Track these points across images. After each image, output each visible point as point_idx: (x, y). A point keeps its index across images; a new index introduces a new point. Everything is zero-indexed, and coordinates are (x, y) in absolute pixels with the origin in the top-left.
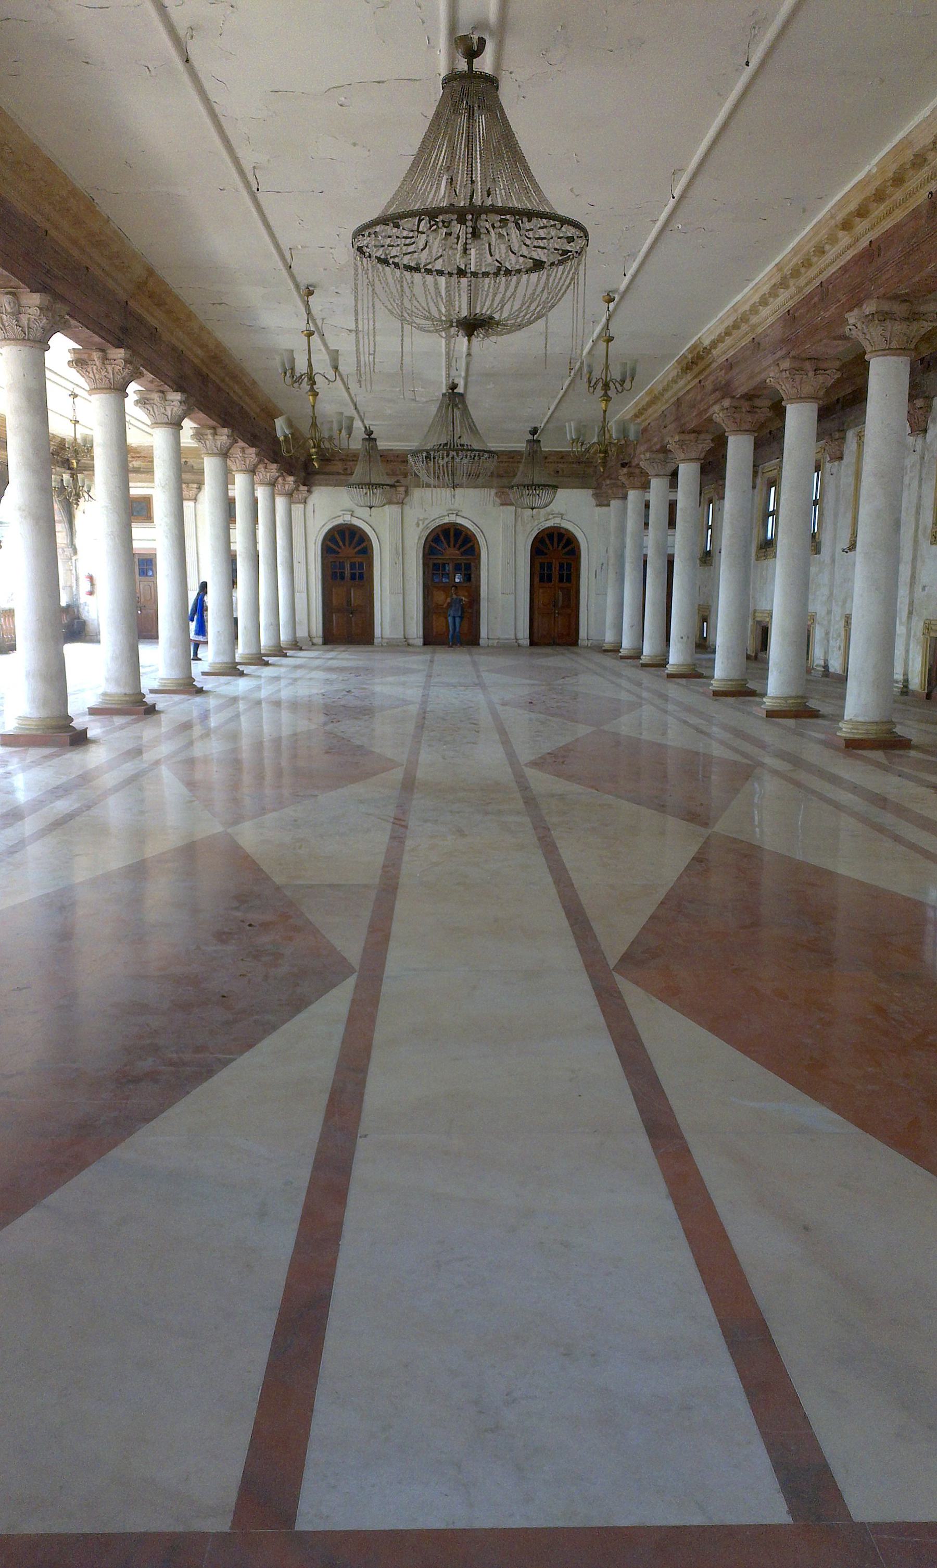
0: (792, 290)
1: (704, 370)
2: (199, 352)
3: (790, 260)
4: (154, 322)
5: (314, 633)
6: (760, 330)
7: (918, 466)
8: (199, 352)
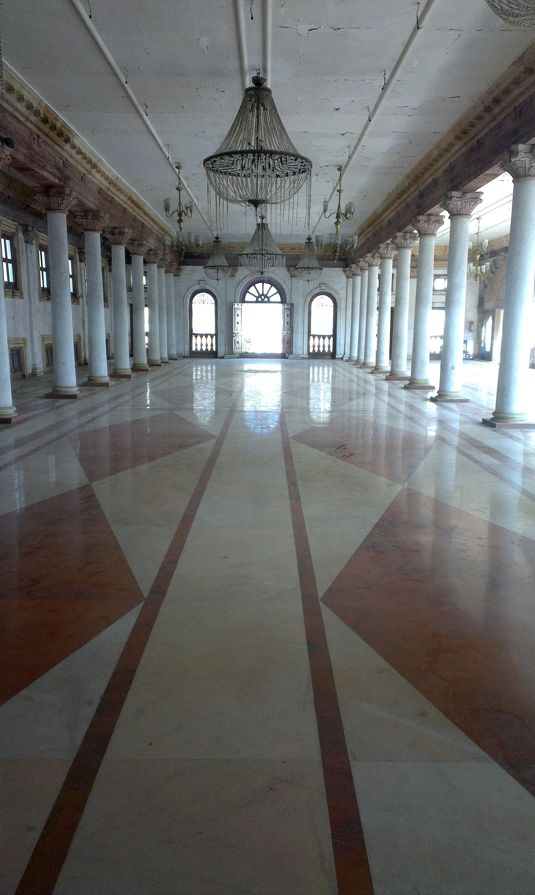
0: (108, 186)
1: (55, 142)
2: (457, 147)
3: (120, 183)
4: (429, 181)
5: (207, 285)
6: (89, 177)
7: (119, 408)
8: (457, 147)
